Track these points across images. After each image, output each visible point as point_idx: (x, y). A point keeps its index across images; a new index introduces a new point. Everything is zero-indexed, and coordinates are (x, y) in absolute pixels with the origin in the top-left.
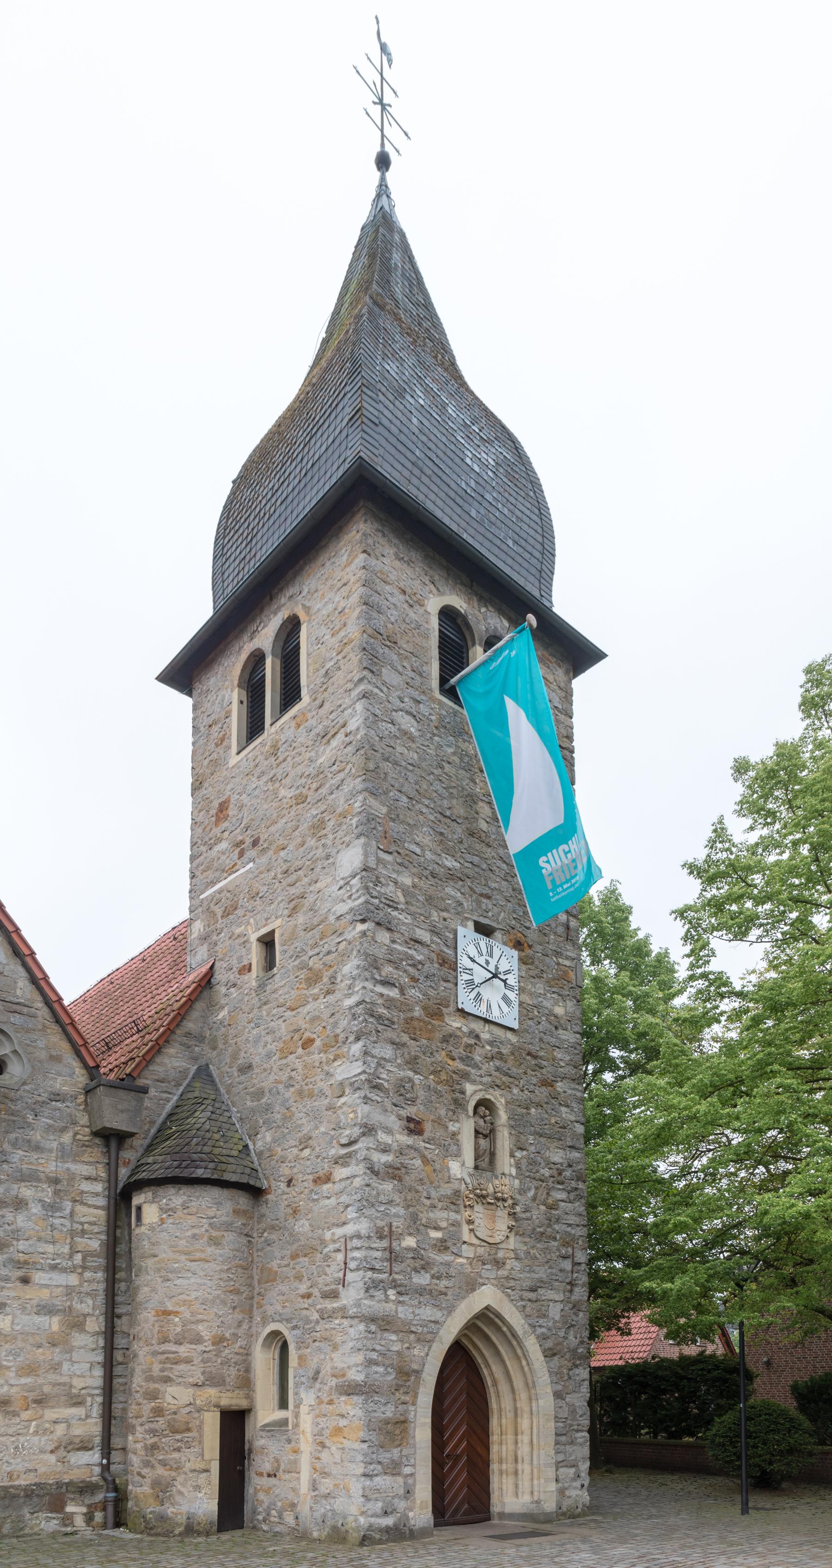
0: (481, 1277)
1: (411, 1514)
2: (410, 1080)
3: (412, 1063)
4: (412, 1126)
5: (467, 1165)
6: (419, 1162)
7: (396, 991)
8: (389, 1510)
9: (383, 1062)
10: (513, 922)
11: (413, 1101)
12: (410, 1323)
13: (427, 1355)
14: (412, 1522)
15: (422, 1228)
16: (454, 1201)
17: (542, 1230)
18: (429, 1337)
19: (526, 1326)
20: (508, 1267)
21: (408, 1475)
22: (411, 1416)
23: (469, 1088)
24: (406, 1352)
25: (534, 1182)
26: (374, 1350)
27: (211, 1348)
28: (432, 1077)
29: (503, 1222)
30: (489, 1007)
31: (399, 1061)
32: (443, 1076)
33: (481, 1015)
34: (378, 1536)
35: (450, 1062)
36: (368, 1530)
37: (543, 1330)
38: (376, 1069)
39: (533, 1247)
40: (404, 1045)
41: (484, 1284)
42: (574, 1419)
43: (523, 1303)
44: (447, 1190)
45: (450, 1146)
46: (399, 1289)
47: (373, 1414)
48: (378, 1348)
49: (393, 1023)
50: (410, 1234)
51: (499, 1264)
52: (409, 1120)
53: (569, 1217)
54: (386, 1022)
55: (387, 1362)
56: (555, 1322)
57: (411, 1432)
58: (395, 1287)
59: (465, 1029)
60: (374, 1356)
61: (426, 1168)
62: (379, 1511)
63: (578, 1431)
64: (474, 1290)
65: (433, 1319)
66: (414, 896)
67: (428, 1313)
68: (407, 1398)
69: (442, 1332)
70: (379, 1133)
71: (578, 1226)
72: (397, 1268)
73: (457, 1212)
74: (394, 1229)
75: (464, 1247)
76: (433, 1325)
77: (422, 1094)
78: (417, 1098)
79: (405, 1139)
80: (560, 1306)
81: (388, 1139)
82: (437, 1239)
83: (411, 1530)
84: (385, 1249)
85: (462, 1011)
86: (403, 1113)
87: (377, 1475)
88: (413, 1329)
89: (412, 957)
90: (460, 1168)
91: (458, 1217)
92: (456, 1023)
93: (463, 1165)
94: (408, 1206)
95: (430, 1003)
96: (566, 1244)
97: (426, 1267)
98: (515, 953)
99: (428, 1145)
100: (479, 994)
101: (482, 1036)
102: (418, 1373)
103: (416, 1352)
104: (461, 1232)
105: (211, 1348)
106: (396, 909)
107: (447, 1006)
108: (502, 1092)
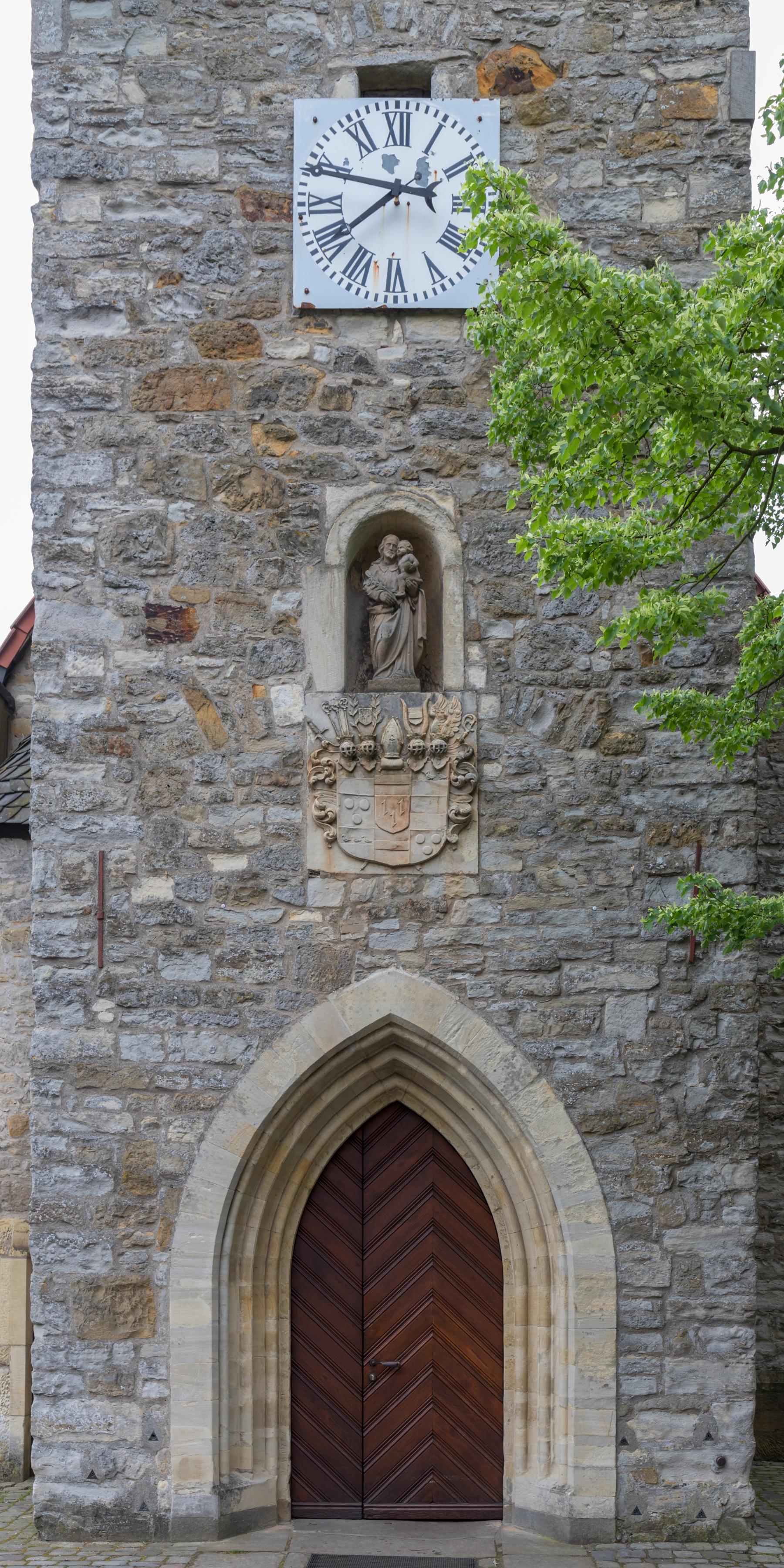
0: (366, 949)
1: (162, 1485)
2: (160, 522)
3: (163, 477)
4: (160, 624)
5: (319, 686)
6: (182, 703)
7: (121, 320)
8: (101, 1471)
9: (78, 495)
10: (496, 25)
11: (164, 566)
12: (156, 1070)
13: (201, 1139)
14: (163, 1503)
15: (189, 853)
16: (284, 778)
17: (581, 813)
18: (209, 1098)
19: (519, 1061)
20: (456, 918)
21: (151, 1402)
22: (159, 1273)
23: (334, 497)
24: (149, 1135)
25: (551, 692)
26: (57, 1132)
27: (11, 1140)
28: (221, 497)
29: (432, 808)
30: (395, 274)
31: (123, 482)
32: (252, 486)
33: (370, 303)
34: (71, 1523)
35: (278, 448)
36: (46, 1508)
37: (583, 1067)
38: (62, 515)
39: (547, 861)
40: (137, 442)
41: (375, 967)
42: (696, 1289)
43: (509, 1004)
44: (264, 755)
45: (277, 649)
46: (122, 998)
47: (57, 1268)
48: (68, 1127)
49: (109, 398)
50: (155, 872)
51: (424, 914)
52: (152, 611)
53: (684, 767)
54: (89, 402)
55: (91, 1157)
56: (623, 1044)
57: (161, 1309)
58: (111, 993)
59: (322, 354)
60: (59, 1144)
61: (201, 715)
62: (77, 1472)
63: (710, 1322)
64: (346, 983)
65: (218, 1057)
66: (172, 74)
67: (204, 1044)
68: (150, 1235)
69: (242, 1087)
70: (70, 656)
71: (718, 785)
72: (116, 950)
73: (293, 804)
74: (110, 865)
75: (314, 884)
76: (219, 1072)
77: (187, 544)
78: (174, 555)
79: (141, 658)
80: (641, 1005)
81: (94, 667)
82: (232, 875)
83: (160, 1521)
84: (86, 913)
85: (306, 311)
86: (136, 599)
87: (70, 1396)
88: (162, 1082)
89: (165, 227)
90: (303, 699)
91: (295, 816)
92: (289, 349)
93: (309, 686)
94: (148, 811)
95: (216, 322)
96: (665, 840)
97: (197, 942)
98: (491, 108)
99: (206, 661)
100: (361, 252)
101: (383, 356)
102: (174, 1179)
103: (172, 1133)
104: (300, 850)
105: (11, 1140)
106: (121, 125)
107: (268, 315)
108: (444, 484)
